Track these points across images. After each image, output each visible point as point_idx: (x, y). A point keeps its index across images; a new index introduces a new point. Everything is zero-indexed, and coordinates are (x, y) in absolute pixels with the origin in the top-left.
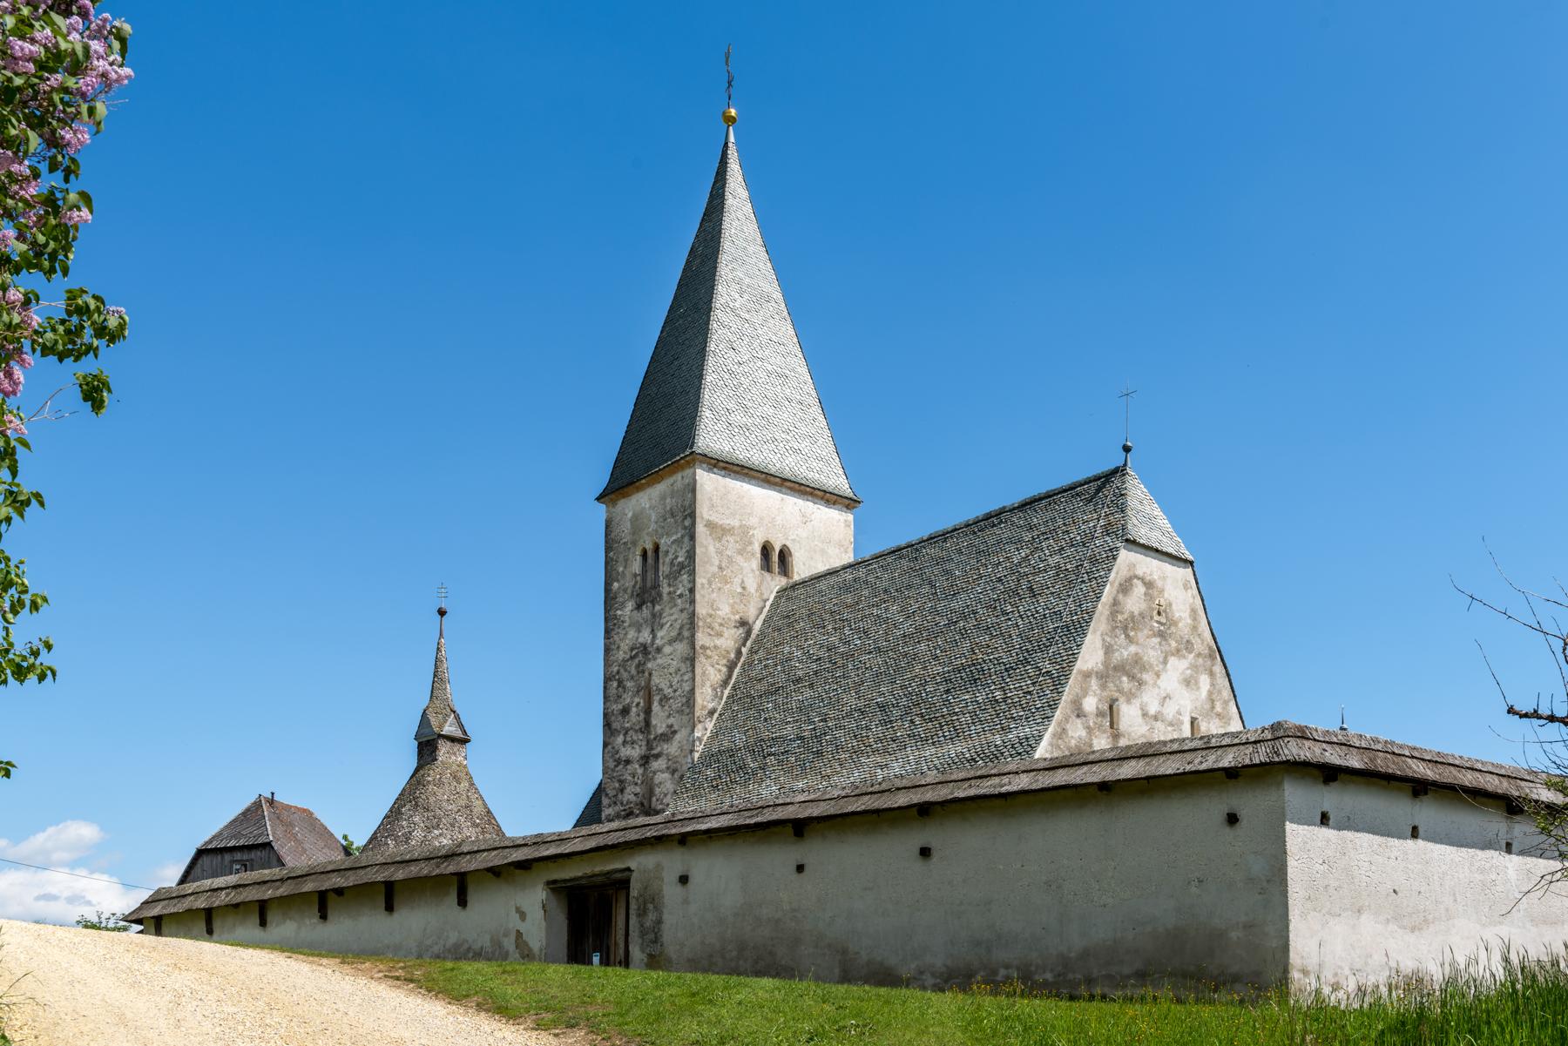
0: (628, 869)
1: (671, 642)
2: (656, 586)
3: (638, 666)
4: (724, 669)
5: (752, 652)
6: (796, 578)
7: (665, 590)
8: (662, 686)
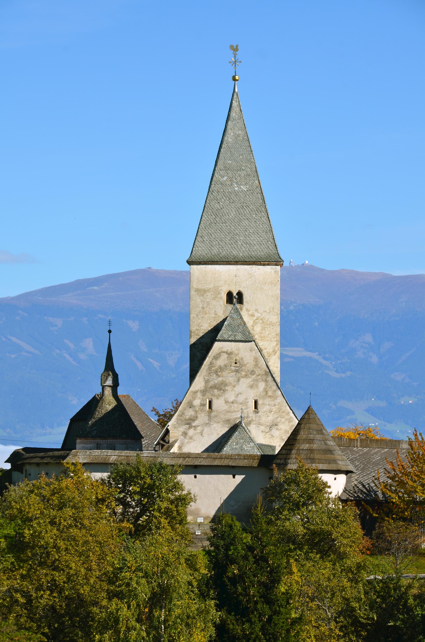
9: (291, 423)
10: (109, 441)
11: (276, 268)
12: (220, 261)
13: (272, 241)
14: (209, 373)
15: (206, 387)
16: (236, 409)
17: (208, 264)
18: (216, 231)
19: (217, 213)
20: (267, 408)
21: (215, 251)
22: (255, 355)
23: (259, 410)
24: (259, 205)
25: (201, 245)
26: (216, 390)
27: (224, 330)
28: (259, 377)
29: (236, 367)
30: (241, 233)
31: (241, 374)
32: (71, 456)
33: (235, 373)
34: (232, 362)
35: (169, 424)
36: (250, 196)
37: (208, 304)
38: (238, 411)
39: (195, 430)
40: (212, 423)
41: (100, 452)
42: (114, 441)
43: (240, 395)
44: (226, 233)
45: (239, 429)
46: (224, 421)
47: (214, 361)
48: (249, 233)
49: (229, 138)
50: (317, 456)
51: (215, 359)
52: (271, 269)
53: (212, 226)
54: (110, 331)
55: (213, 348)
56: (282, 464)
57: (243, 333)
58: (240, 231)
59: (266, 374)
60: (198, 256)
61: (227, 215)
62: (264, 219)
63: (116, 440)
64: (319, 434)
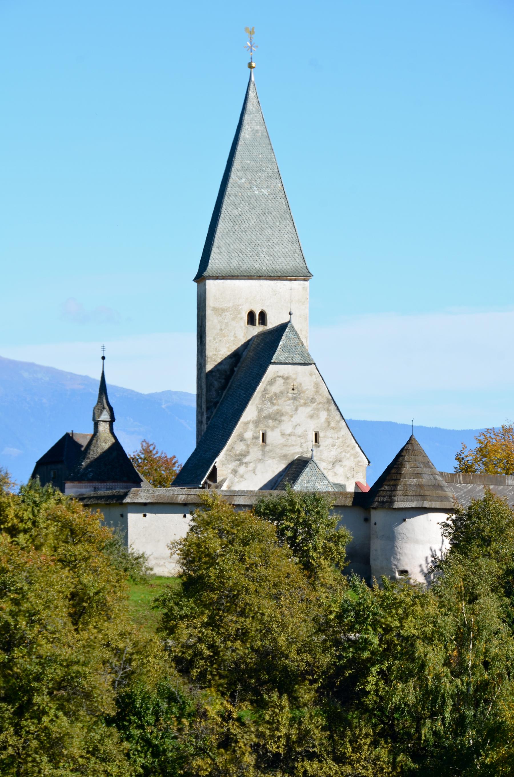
4: (223, 381)
9: (357, 459)
10: (108, 484)
11: (304, 284)
12: (242, 276)
13: (299, 253)
14: (263, 401)
15: (259, 417)
16: (293, 443)
17: (227, 279)
18: (235, 241)
19: (236, 220)
20: (329, 441)
21: (234, 264)
22: (315, 380)
23: (320, 443)
24: (283, 211)
25: (217, 257)
26: (270, 421)
27: (280, 351)
28: (321, 405)
29: (294, 394)
30: (264, 244)
31: (300, 402)
32: (131, 495)
33: (292, 401)
34: (289, 388)
35: (217, 460)
36: (273, 201)
37: (227, 324)
38: (296, 445)
39: (247, 467)
40: (266, 459)
41: (165, 491)
42: (114, 484)
43: (298, 426)
44: (247, 244)
45: (310, 465)
46: (280, 456)
47: (268, 387)
48: (273, 244)
49: (245, 134)
50: (428, 493)
51: (269, 384)
52: (299, 285)
53: (229, 235)
54: (103, 358)
55: (267, 372)
56: (387, 502)
57: (302, 356)
58: (262, 242)
59: (328, 402)
60: (214, 269)
61: (246, 222)
62: (289, 228)
63: (116, 484)
64: (426, 467)
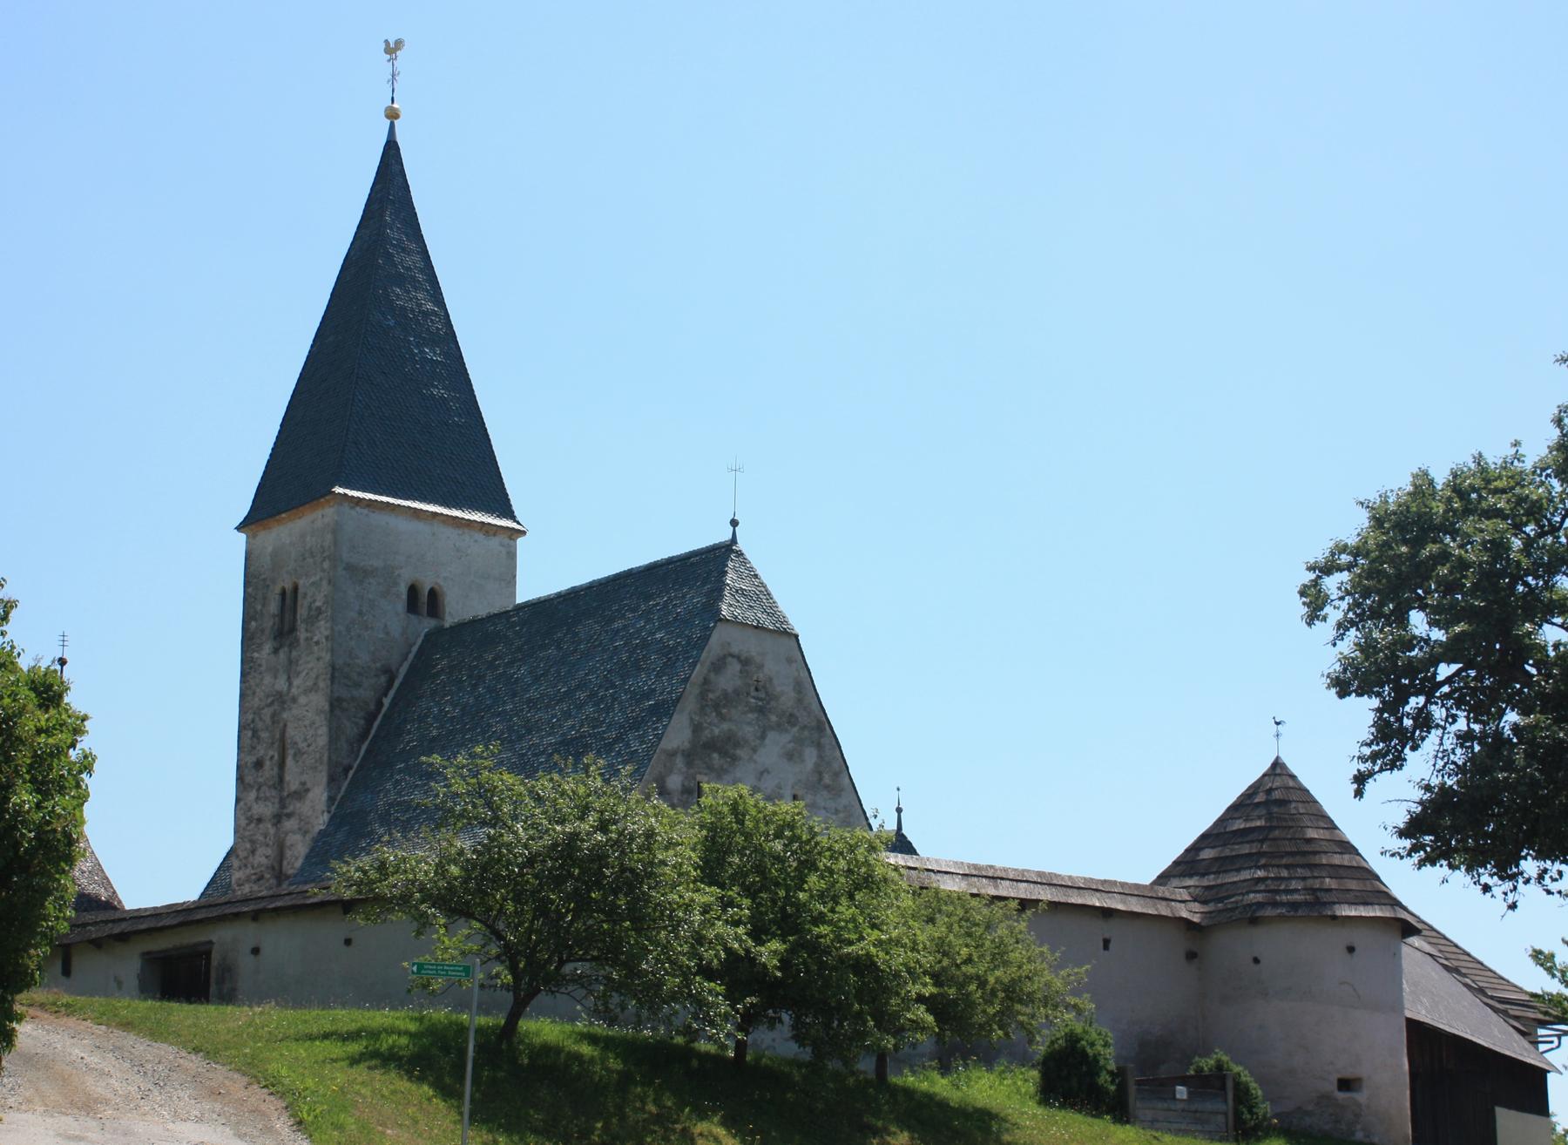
0: (211, 943)
1: (307, 691)
2: (293, 629)
3: (274, 715)
4: (362, 722)
5: (394, 704)
6: (448, 622)
7: (302, 634)
8: (297, 739)
